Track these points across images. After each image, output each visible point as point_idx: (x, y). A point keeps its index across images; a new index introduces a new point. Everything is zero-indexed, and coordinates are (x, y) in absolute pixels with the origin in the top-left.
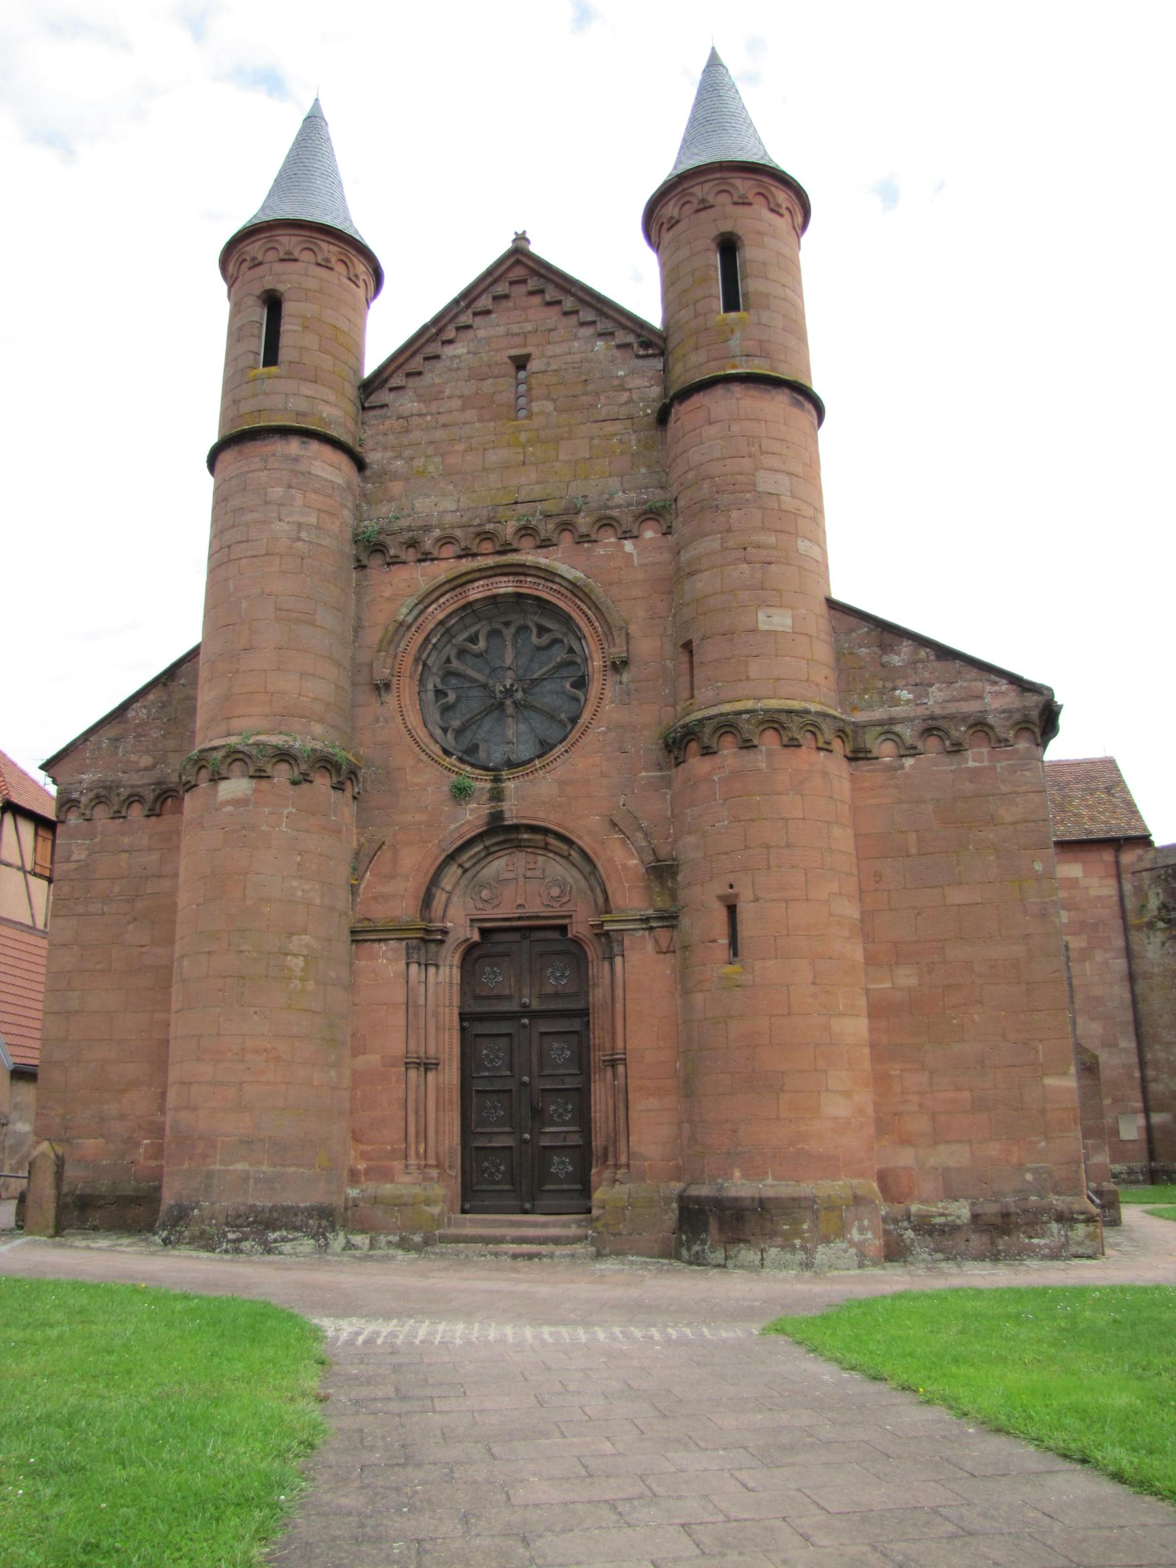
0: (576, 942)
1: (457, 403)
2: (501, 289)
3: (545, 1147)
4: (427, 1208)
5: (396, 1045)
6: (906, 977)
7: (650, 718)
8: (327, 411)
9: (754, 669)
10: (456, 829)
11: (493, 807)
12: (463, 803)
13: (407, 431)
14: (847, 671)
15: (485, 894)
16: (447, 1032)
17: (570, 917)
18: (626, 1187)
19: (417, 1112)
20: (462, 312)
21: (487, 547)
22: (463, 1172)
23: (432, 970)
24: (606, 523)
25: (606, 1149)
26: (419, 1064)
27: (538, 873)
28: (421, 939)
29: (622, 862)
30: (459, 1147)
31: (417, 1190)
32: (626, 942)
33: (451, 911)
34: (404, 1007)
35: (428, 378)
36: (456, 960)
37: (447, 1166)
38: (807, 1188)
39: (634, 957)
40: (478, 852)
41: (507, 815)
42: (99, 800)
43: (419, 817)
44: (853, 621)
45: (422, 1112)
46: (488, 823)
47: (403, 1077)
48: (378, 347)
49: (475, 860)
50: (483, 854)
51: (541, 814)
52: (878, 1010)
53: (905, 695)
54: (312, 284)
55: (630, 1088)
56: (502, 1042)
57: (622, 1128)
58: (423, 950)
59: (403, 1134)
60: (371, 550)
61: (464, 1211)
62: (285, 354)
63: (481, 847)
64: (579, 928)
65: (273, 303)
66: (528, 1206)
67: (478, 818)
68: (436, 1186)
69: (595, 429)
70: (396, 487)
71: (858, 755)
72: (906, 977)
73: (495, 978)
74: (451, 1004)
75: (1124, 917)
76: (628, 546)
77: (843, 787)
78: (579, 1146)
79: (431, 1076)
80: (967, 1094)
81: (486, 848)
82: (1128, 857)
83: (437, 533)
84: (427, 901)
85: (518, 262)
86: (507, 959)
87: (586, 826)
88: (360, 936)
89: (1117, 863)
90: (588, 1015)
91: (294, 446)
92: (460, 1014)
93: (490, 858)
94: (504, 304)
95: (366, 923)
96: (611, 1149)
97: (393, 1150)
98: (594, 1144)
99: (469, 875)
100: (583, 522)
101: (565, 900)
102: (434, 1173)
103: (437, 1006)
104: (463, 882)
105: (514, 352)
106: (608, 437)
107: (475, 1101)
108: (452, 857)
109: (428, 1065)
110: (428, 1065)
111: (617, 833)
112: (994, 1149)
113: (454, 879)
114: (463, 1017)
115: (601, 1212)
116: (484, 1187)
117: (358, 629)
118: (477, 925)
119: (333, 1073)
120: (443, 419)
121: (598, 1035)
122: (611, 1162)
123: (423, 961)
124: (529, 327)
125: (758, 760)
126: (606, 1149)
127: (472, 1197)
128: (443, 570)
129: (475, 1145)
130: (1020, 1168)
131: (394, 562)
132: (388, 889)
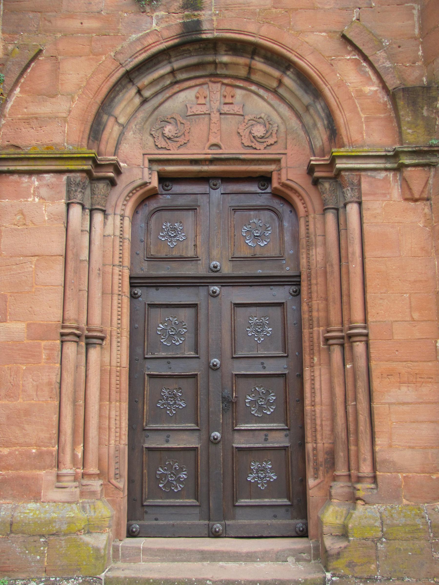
0: (283, 196)
3: (240, 449)
4: (87, 538)
5: (49, 310)
10: (138, 40)
11: (187, 16)
12: (148, 9)
15: (169, 130)
16: (115, 297)
17: (278, 161)
18: (375, 509)
19: (75, 402)
22: (130, 481)
23: (98, 217)
25: (331, 455)
26: (78, 336)
27: (236, 109)
28: (88, 172)
30: (127, 447)
31: (74, 512)
32: (364, 186)
33: (125, 148)
34: (62, 259)
37: (112, 474)
39: (374, 206)
40: (162, 77)
41: (206, 26)
43: (92, 24)
45: (81, 402)
46: (180, 35)
47: (57, 353)
49: (158, 88)
50: (168, 82)
51: (251, 28)
55: (375, 374)
56: (185, 315)
57: (364, 426)
58: (88, 192)
59: (55, 431)
61: (131, 534)
63: (167, 69)
64: (291, 173)
66: (218, 526)
67: (168, 28)
68: (99, 504)
74: (121, 265)
78: (285, 448)
79: (94, 353)
81: (173, 72)
84: (96, 131)
86: (191, 213)
87: (309, 42)
90: (298, 284)
92: (131, 278)
93: (176, 88)
95: (12, 150)
96: (341, 455)
97: (40, 455)
98: (309, 446)
99: (148, 106)
101: (271, 141)
102: (96, 485)
103: (104, 265)
104: (141, 115)
107: (147, 388)
108: (129, 77)
109: (90, 339)
110: (90, 339)
111: (349, 53)
113: (130, 110)
114: (135, 282)
115: (343, 544)
116: (159, 501)
118: (157, 167)
121: (317, 303)
122: (341, 471)
123: (88, 206)
126: (331, 455)
127: (142, 514)
129: (146, 445)
132: (45, 109)
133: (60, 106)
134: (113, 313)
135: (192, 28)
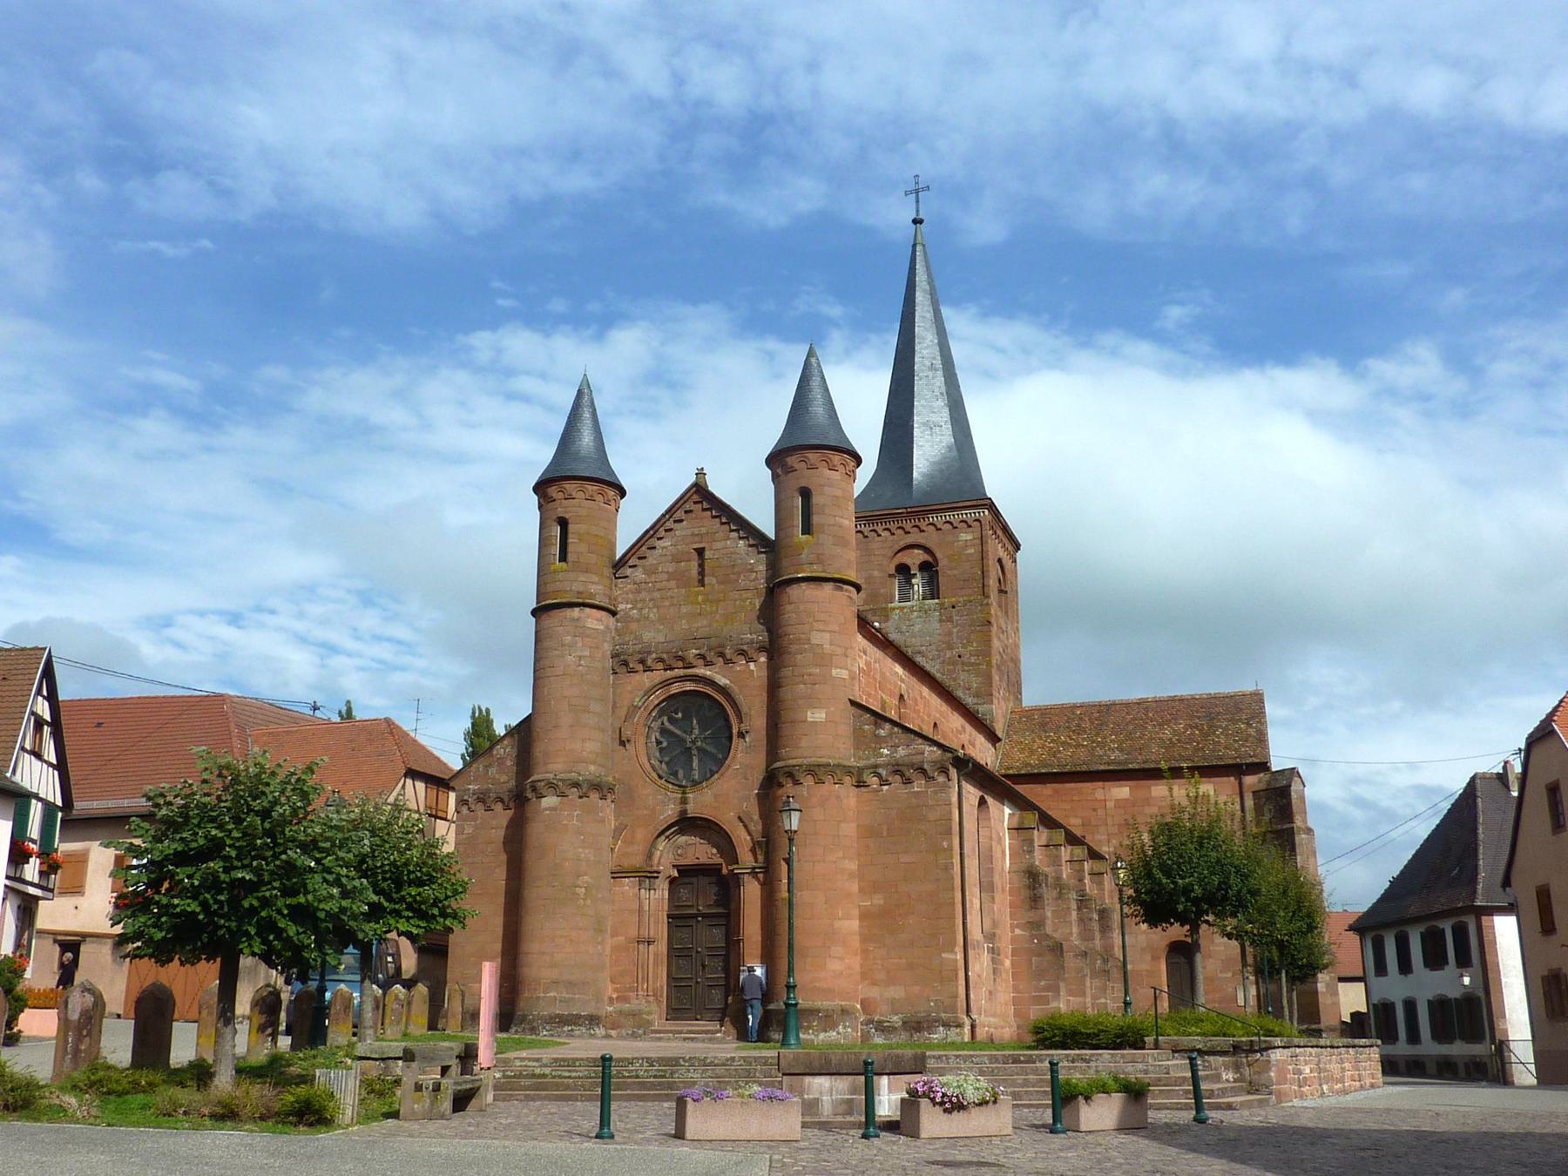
5: (633, 933)
6: (878, 900)
8: (593, 589)
9: (804, 743)
13: (639, 592)
14: (859, 740)
21: (680, 664)
29: (742, 840)
36: (666, 886)
38: (818, 1004)
48: (624, 540)
52: (865, 916)
54: (584, 512)
60: (622, 663)
62: (570, 557)
69: (735, 595)
71: (860, 784)
72: (878, 900)
73: (684, 893)
76: (752, 666)
77: (852, 802)
82: (1250, 780)
89: (1240, 784)
91: (576, 611)
112: (917, 989)
117: (614, 707)
120: (658, 586)
124: (704, 530)
125: (803, 791)
128: (659, 675)
134: (660, 931)
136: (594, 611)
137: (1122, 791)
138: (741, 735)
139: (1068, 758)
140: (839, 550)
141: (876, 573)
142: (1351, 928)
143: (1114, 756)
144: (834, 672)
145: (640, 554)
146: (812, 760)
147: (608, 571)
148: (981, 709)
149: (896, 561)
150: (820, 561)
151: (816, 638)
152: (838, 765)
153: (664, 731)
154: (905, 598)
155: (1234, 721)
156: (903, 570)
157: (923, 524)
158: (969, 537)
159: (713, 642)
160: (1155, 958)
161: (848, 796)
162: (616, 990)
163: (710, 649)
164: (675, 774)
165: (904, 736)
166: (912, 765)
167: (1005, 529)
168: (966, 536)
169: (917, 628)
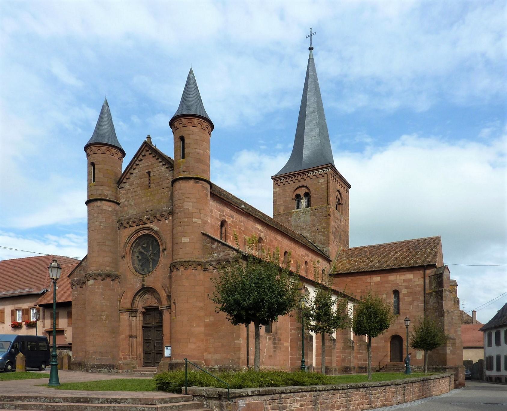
1: (137, 185)
2: (144, 153)
5: (127, 333)
7: (169, 262)
8: (106, 193)
9: (181, 252)
20: (136, 160)
21: (141, 223)
24: (162, 216)
29: (163, 294)
35: (131, 180)
36: (141, 315)
42: (78, 284)
44: (206, 238)
52: (207, 326)
53: (215, 255)
65: (93, 164)
69: (161, 191)
70: (126, 208)
75: (424, 291)
80: (220, 344)
82: (429, 272)
83: (132, 220)
84: (133, 303)
85: (146, 146)
87: (158, 287)
88: (122, 311)
89: (424, 273)
91: (99, 203)
94: (145, 157)
100: (158, 216)
105: (147, 171)
106: (164, 193)
119: (114, 339)
120: (134, 190)
124: (150, 163)
125: (179, 273)
128: (134, 228)
130: (229, 359)
131: (125, 228)
133: (127, 301)
134: (139, 333)
135: (143, 285)
136: (107, 202)
137: (377, 279)
138: (164, 251)
139: (358, 267)
140: (197, 164)
141: (288, 199)
142: (481, 330)
143: (377, 265)
144: (194, 220)
145: (127, 177)
146: (183, 260)
147: (114, 185)
148: (325, 249)
149: (295, 194)
150: (188, 170)
151: (186, 205)
152: (194, 261)
153: (140, 253)
154: (299, 207)
155: (425, 249)
156: (298, 196)
157: (305, 177)
158: (323, 181)
159: (153, 212)
160: (386, 341)
161: (199, 274)
162: (123, 355)
163: (151, 215)
164: (143, 270)
165: (222, 248)
166: (224, 260)
167: (341, 178)
168: (321, 180)
169: (302, 219)
